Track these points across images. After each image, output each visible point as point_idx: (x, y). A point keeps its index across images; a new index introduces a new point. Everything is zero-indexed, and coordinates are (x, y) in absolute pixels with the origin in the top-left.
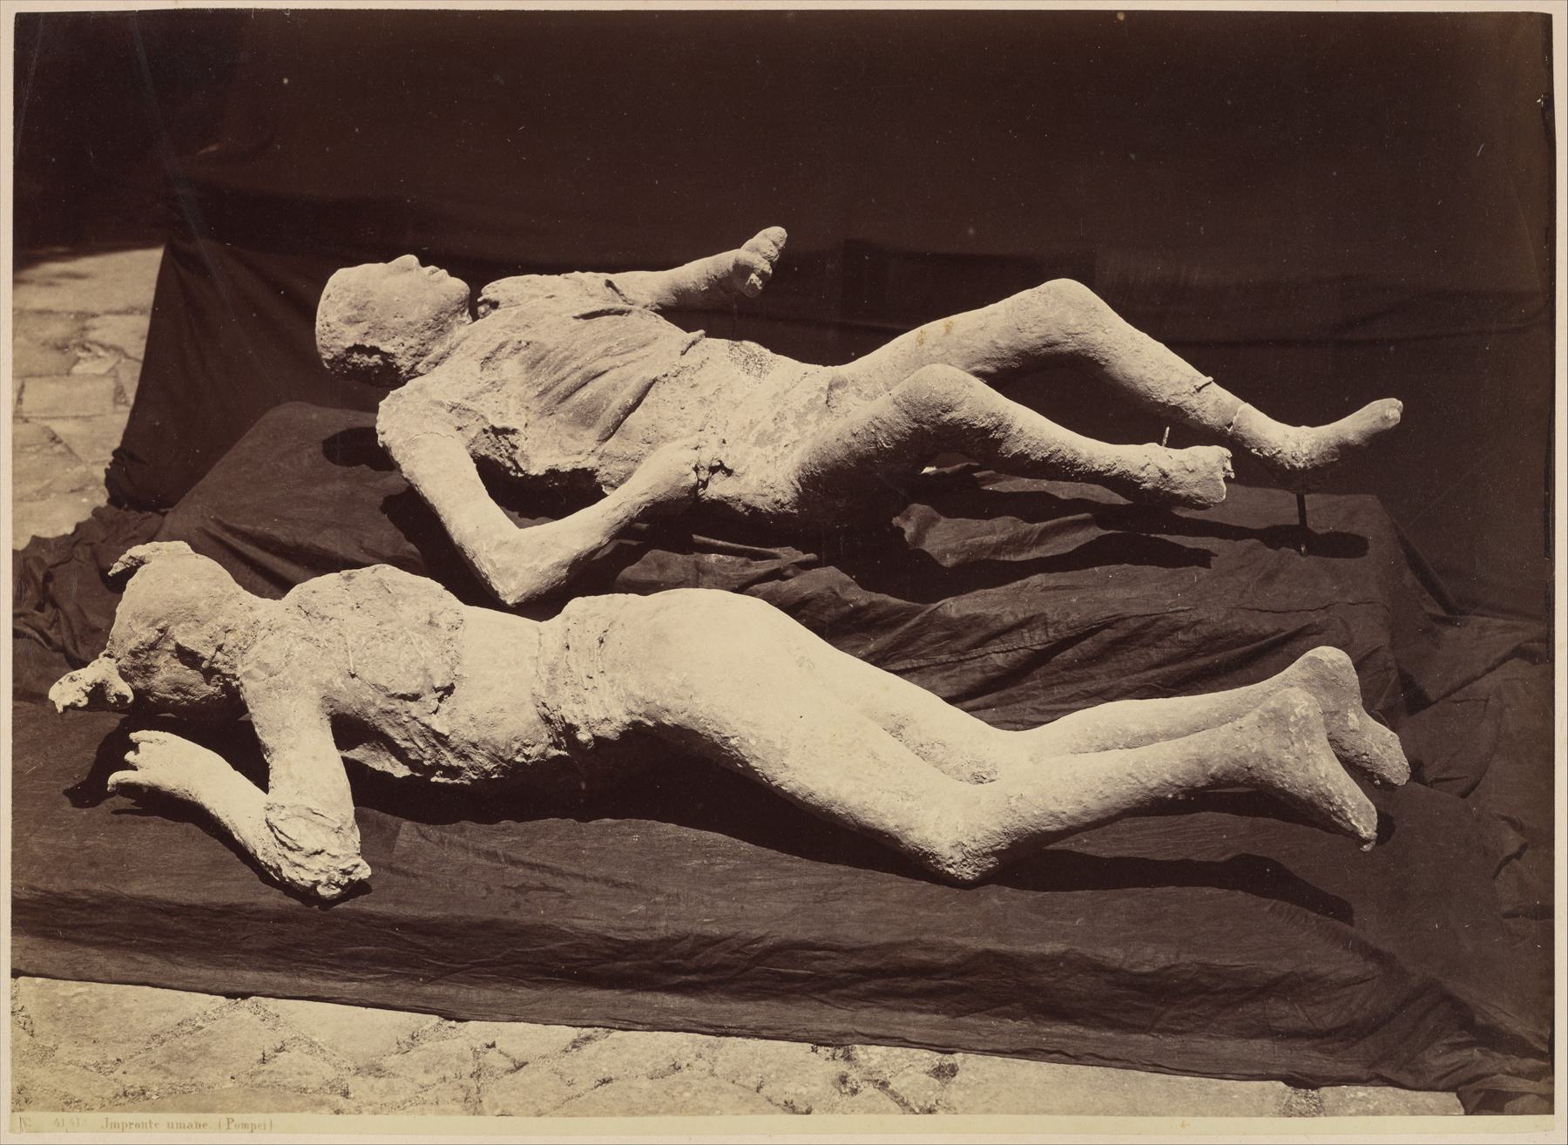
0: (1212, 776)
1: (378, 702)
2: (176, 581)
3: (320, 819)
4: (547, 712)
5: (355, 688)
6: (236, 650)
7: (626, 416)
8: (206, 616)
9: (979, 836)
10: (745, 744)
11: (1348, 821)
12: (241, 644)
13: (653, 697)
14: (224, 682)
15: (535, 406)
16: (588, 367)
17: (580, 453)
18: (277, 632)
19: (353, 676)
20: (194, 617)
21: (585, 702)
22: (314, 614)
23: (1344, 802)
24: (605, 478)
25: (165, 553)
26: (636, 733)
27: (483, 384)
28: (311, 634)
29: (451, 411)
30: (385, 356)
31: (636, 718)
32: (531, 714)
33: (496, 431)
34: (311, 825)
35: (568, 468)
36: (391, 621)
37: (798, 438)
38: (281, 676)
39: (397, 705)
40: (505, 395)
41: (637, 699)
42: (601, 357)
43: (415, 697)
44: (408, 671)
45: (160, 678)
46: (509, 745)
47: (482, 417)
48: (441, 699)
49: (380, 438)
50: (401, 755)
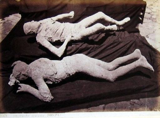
20: (23, 70)
30: (33, 32)
39: (51, 76)
43: (53, 75)
50: (52, 81)
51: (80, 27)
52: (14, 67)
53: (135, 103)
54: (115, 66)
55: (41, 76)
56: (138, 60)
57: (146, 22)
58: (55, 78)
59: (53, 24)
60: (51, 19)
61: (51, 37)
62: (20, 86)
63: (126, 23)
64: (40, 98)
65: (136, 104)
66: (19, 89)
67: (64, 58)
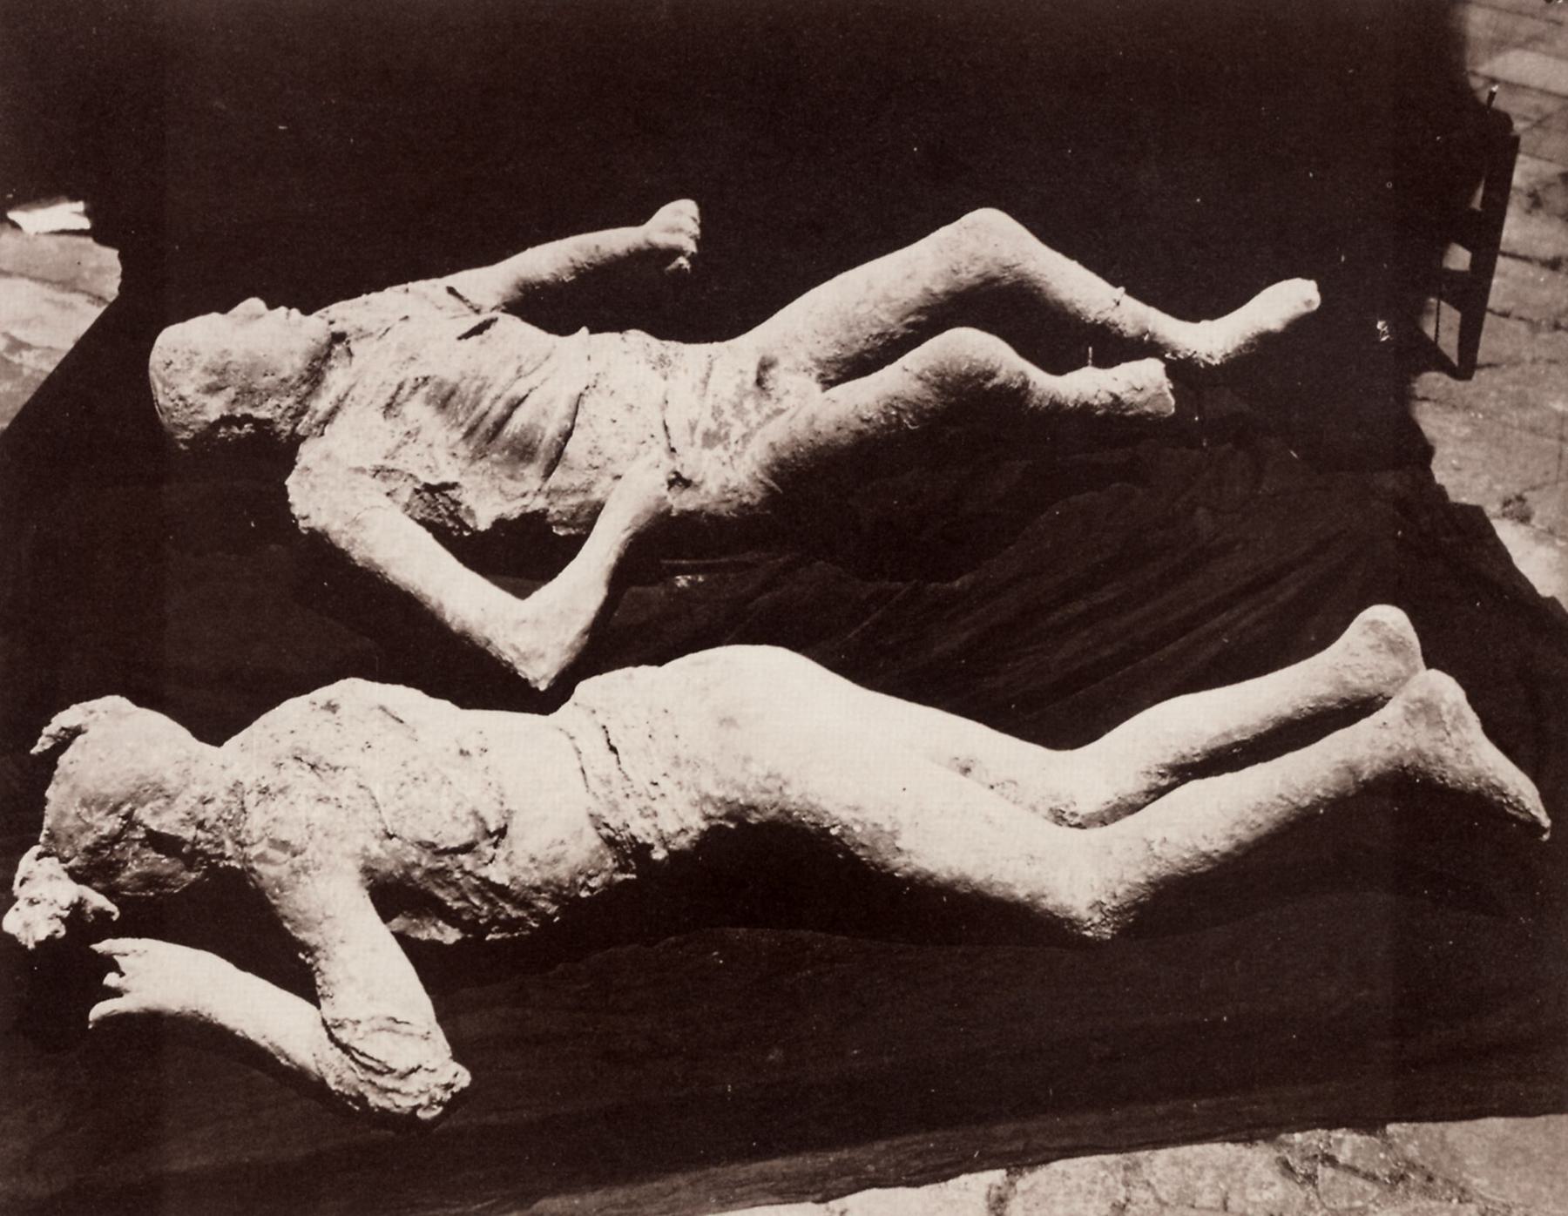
0: (1365, 782)
1: (423, 862)
2: (132, 752)
3: (404, 1028)
4: (612, 834)
5: (395, 850)
6: (220, 823)
7: (566, 440)
8: (177, 789)
9: (1120, 891)
10: (847, 832)
11: (1527, 812)
12: (225, 816)
13: (734, 795)
14: (210, 864)
15: (463, 451)
16: (508, 395)
17: (524, 495)
18: (280, 797)
19: (391, 837)
20: (160, 792)
21: (655, 814)
22: (322, 766)
23: (1520, 792)
24: (556, 518)
25: (103, 716)
26: (712, 838)
27: (398, 438)
28: (327, 793)
29: (374, 476)
30: (258, 423)
31: (714, 823)
32: (592, 840)
33: (428, 488)
34: (396, 1037)
35: (516, 515)
36: (415, 758)
37: (745, 430)
38: (308, 855)
40: (424, 445)
41: (715, 800)
42: (515, 380)
44: (455, 819)
45: (128, 873)
46: (573, 881)
47: (411, 475)
48: (496, 845)
49: (302, 524)
50: (452, 918)
51: (760, 382)
52: (63, 760)
53: (1330, 1160)
54: (1131, 784)
55: (344, 855)
56: (1378, 717)
57: (1515, 362)
58: (485, 880)
59: (467, 336)
60: (451, 291)
61: (450, 478)
62: (109, 963)
63: (1265, 342)
64: (331, 1081)
65: (1342, 1177)
66: (117, 993)
67: (587, 690)
